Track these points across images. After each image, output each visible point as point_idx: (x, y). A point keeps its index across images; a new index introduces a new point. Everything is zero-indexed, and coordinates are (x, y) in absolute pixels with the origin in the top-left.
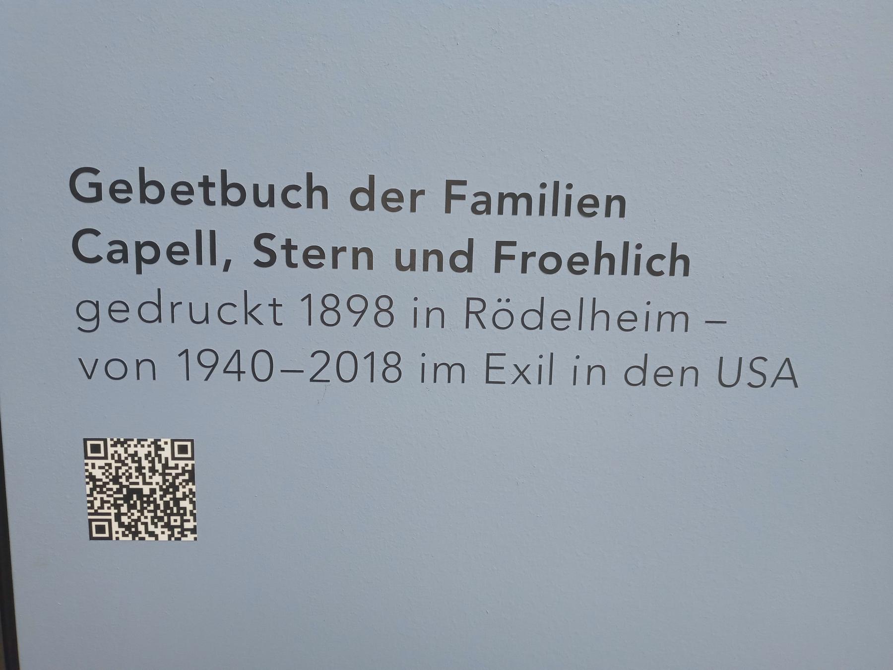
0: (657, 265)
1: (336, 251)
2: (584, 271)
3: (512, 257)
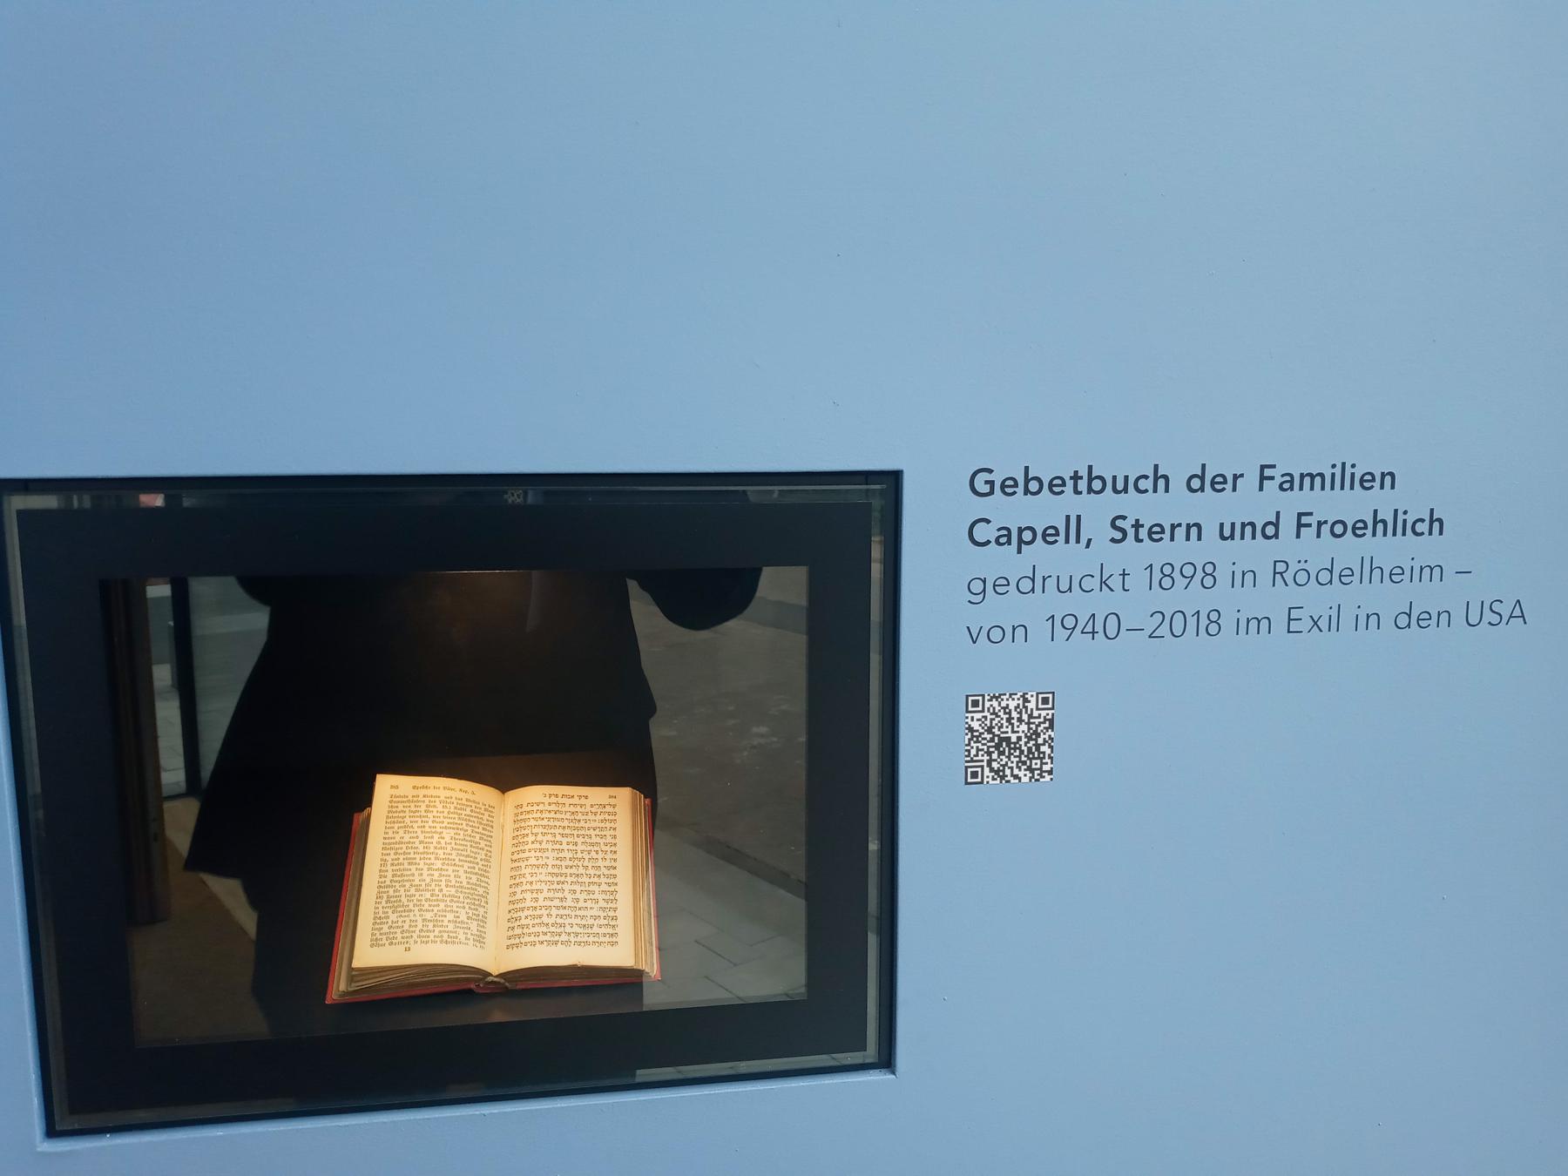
3: (1309, 525)
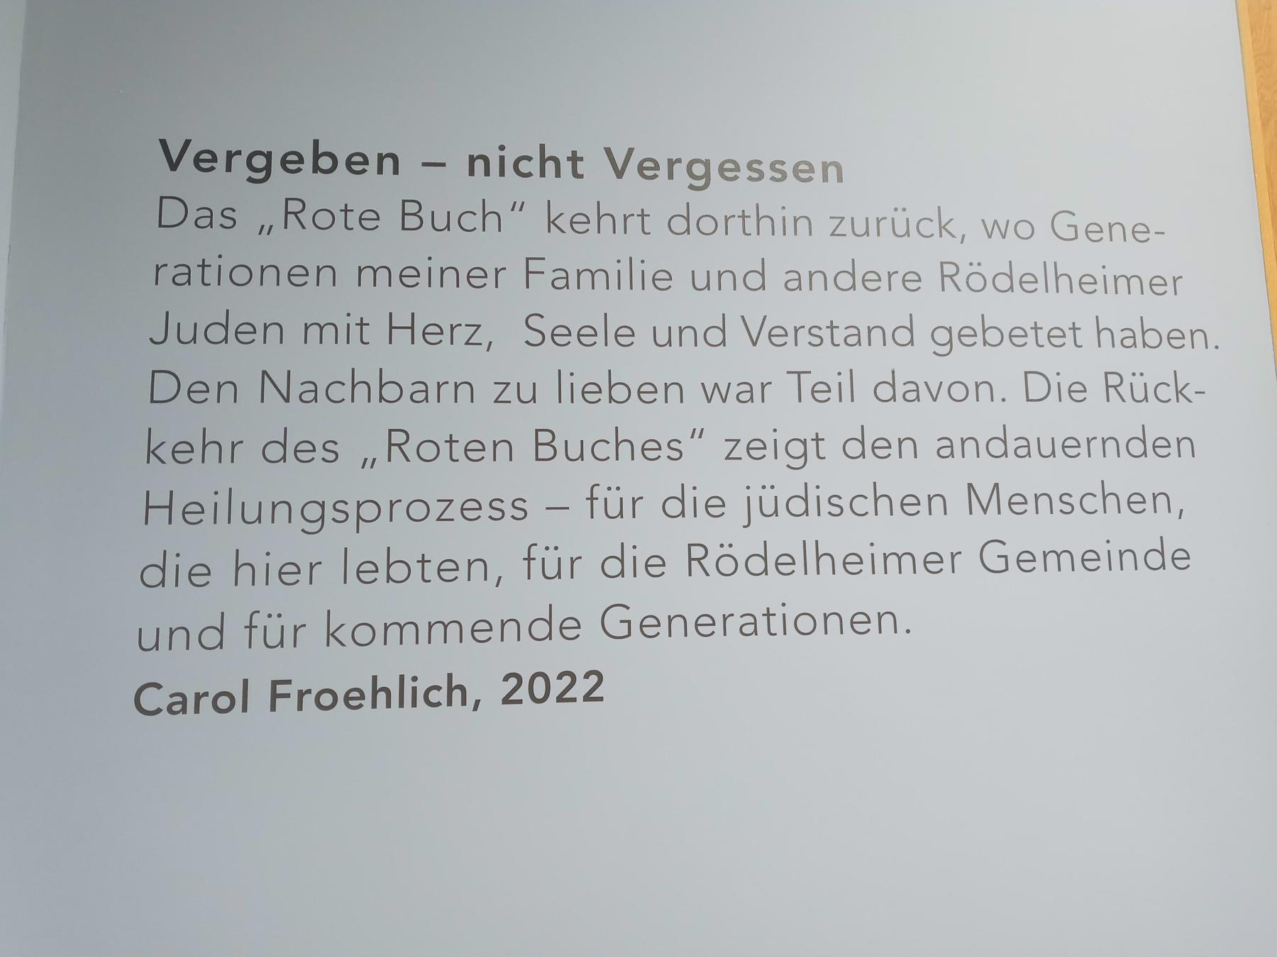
0: (434, 696)
1: (198, 697)
2: (361, 706)
3: (287, 696)
